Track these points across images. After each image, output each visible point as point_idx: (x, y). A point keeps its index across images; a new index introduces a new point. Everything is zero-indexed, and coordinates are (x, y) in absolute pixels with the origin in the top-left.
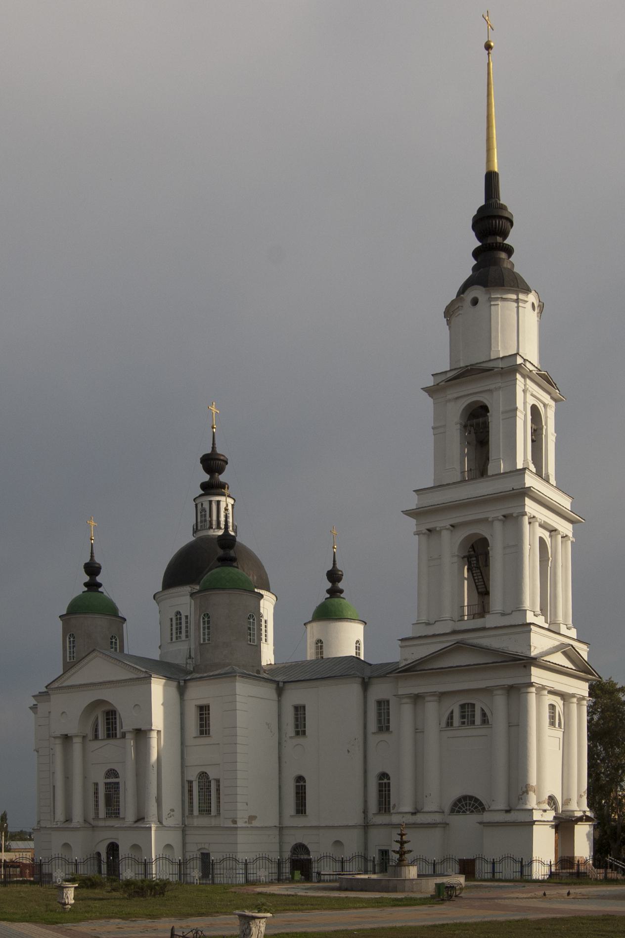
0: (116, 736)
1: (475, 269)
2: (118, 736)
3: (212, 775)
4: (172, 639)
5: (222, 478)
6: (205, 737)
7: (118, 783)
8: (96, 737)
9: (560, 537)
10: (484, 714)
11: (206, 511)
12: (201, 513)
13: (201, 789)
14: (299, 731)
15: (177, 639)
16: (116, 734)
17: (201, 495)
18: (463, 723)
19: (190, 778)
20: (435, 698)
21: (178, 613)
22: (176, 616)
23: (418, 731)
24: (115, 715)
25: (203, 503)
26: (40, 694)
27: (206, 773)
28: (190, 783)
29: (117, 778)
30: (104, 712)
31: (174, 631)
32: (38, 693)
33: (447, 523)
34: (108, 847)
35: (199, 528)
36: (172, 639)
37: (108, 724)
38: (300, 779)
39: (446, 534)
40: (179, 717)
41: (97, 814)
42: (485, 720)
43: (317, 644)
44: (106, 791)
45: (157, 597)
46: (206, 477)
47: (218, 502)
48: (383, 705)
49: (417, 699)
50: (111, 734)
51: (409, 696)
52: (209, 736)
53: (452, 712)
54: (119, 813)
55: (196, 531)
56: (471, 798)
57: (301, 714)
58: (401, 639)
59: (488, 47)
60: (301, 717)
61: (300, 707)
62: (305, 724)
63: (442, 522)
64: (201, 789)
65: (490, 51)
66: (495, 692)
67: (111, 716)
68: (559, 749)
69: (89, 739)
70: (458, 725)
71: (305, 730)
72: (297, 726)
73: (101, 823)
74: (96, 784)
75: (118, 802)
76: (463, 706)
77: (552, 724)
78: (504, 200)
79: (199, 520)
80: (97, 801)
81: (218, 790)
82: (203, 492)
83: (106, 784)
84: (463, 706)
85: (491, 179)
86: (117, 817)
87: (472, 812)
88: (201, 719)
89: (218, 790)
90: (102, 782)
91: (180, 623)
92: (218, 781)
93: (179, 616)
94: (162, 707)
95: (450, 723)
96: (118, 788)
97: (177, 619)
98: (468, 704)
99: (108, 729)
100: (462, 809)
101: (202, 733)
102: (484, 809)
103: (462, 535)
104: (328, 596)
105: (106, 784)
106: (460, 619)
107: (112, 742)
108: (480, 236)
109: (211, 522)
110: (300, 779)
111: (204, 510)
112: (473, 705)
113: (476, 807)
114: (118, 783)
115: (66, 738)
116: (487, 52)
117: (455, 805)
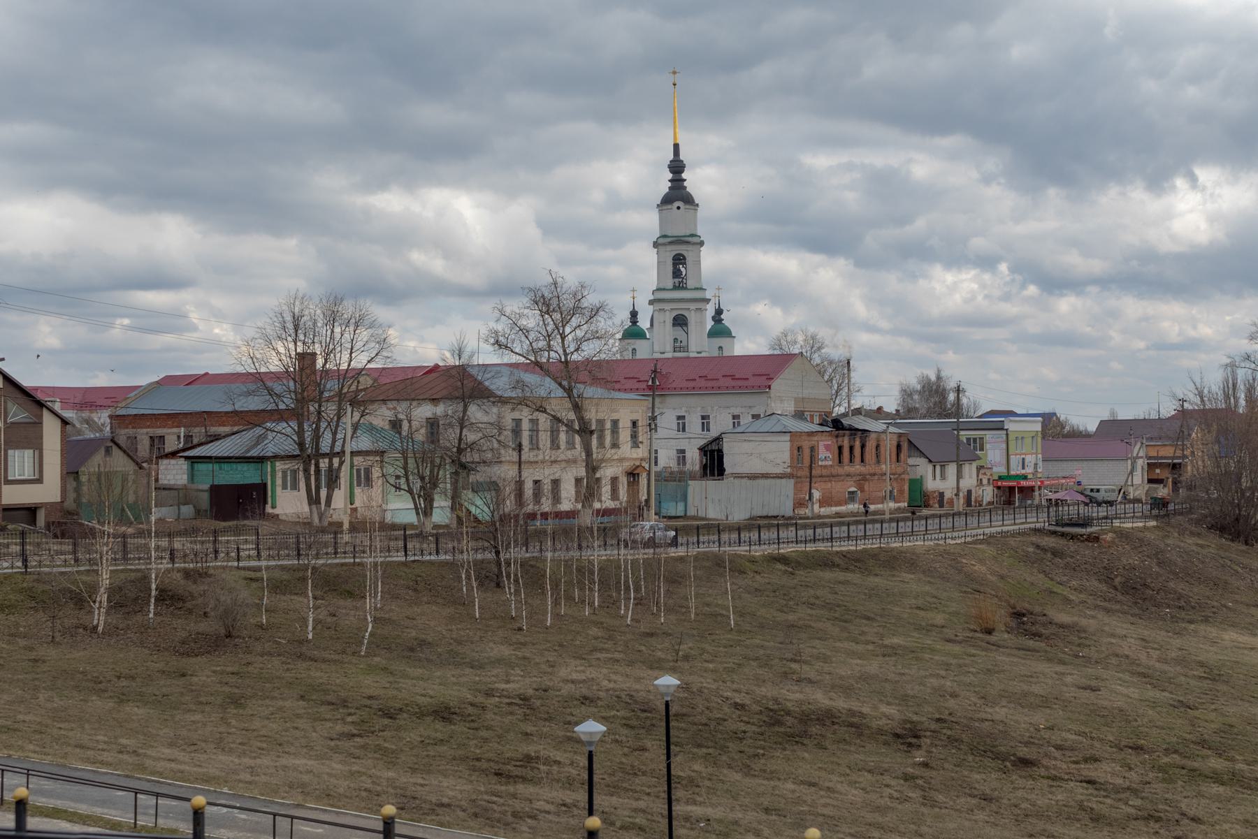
78: (682, 158)
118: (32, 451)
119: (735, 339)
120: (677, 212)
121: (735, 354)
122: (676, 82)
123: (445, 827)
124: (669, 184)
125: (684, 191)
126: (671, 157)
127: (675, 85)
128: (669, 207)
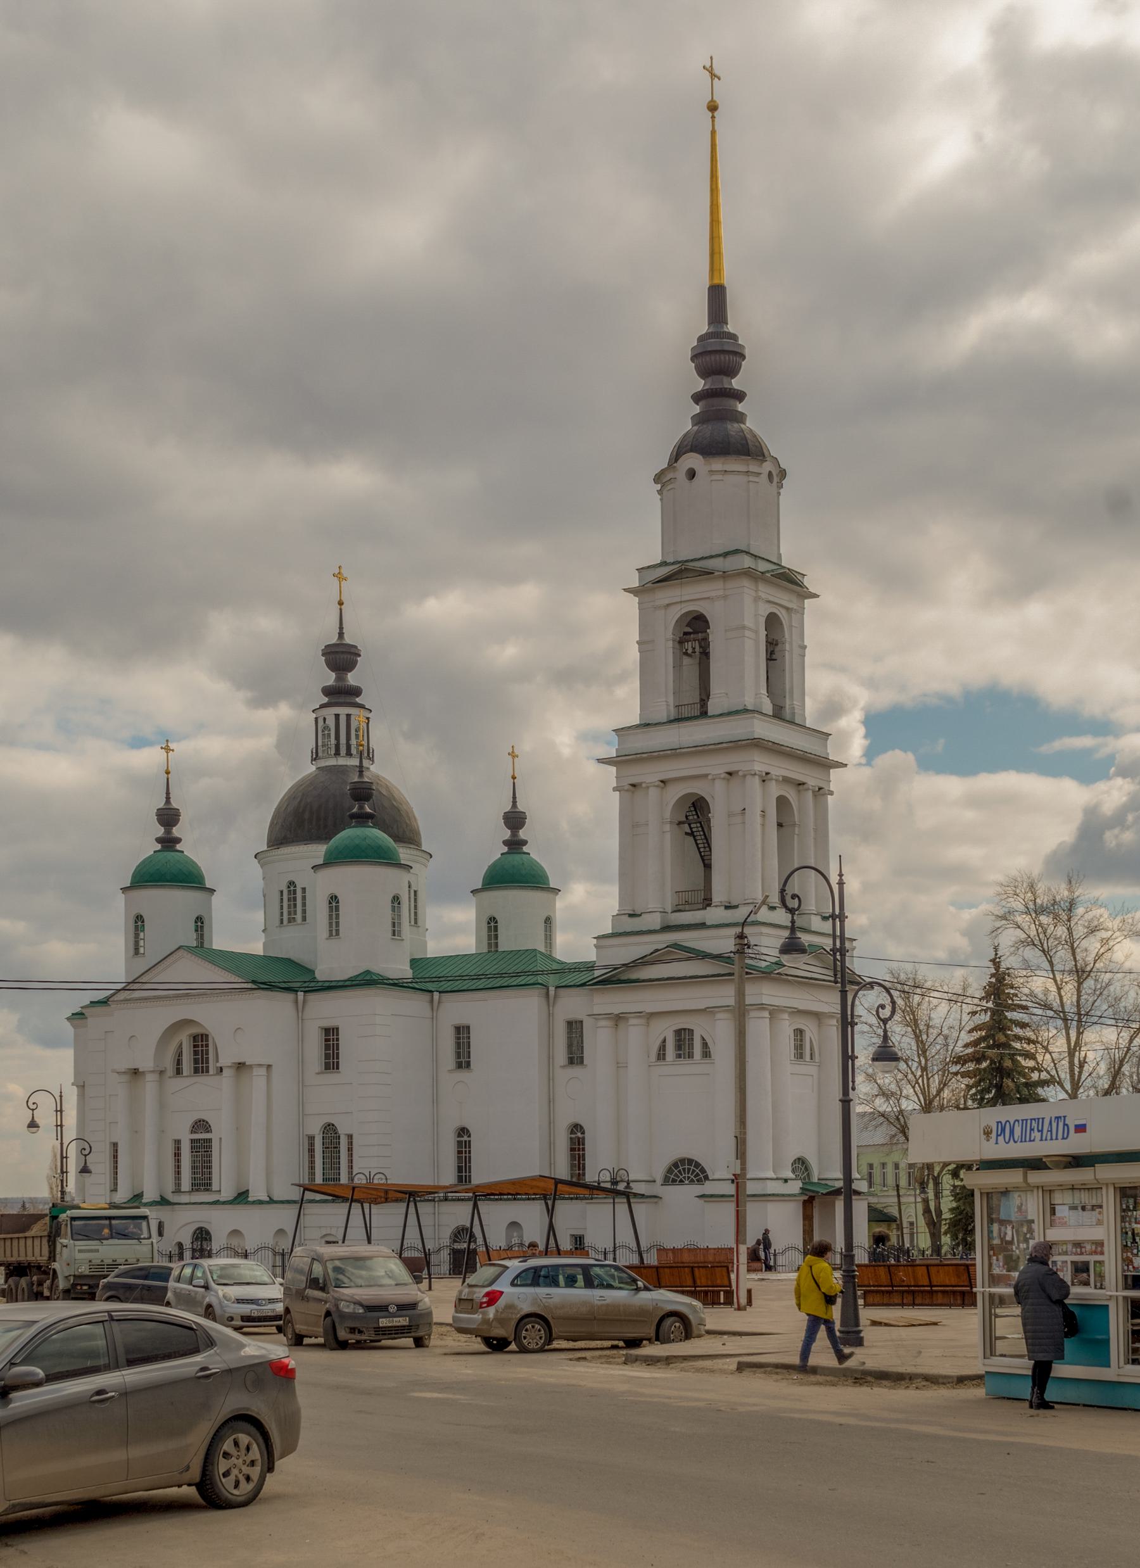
0: (207, 1071)
1: (698, 420)
2: (211, 1071)
3: (342, 1130)
4: (282, 921)
5: (352, 679)
6: (332, 1072)
7: (210, 1140)
8: (179, 1072)
9: (810, 793)
10: (705, 1045)
11: (330, 730)
12: (323, 731)
13: (337, 1148)
14: (462, 1062)
15: (289, 921)
16: (207, 1068)
17: (322, 706)
18: (679, 1056)
19: (310, 1133)
20: (642, 1021)
21: (292, 883)
22: (289, 887)
23: (620, 1065)
24: (207, 1040)
25: (326, 717)
26: (92, 1005)
27: (333, 1125)
28: (311, 1139)
29: (208, 1132)
30: (190, 1036)
33: (654, 778)
34: (195, 1233)
35: (320, 754)
36: (282, 921)
37: (196, 1053)
38: (463, 1131)
39: (653, 793)
41: (178, 1184)
42: (706, 1052)
43: (489, 923)
44: (192, 1152)
45: (259, 857)
46: (330, 678)
48: (574, 1028)
49: (618, 1019)
50: (201, 1066)
51: (608, 1016)
52: (338, 1072)
53: (664, 1041)
54: (210, 1184)
55: (315, 758)
56: (690, 1161)
57: (463, 1038)
58: (596, 936)
59: (713, 108)
60: (463, 1042)
61: (463, 1027)
62: (469, 1052)
63: (650, 774)
64: (337, 1148)
65: (716, 114)
66: (719, 1016)
67: (201, 1042)
68: (813, 1091)
69: (169, 1075)
70: (672, 1060)
71: (470, 1061)
72: (458, 1055)
73: (185, 1198)
74: (178, 1143)
75: (193, 1168)
76: (678, 1032)
77: (800, 1055)
79: (320, 743)
80: (179, 1167)
81: (350, 1150)
83: (192, 1141)
84: (678, 1032)
86: (208, 1190)
87: (692, 1181)
88: (327, 1047)
89: (350, 1150)
90: (186, 1138)
91: (295, 899)
92: (350, 1137)
93: (292, 888)
95: (661, 1055)
96: (210, 1147)
97: (289, 892)
98: (685, 1029)
99: (196, 1061)
100: (679, 1177)
101: (327, 1067)
102: (706, 1178)
103: (675, 793)
104: (506, 849)
105: (192, 1141)
106: (675, 909)
107: (201, 1079)
108: (704, 372)
109: (337, 746)
110: (463, 1131)
111: (326, 728)
112: (691, 1031)
113: (697, 1175)
114: (210, 1140)
115: (136, 1073)
116: (711, 114)
117: (670, 1171)
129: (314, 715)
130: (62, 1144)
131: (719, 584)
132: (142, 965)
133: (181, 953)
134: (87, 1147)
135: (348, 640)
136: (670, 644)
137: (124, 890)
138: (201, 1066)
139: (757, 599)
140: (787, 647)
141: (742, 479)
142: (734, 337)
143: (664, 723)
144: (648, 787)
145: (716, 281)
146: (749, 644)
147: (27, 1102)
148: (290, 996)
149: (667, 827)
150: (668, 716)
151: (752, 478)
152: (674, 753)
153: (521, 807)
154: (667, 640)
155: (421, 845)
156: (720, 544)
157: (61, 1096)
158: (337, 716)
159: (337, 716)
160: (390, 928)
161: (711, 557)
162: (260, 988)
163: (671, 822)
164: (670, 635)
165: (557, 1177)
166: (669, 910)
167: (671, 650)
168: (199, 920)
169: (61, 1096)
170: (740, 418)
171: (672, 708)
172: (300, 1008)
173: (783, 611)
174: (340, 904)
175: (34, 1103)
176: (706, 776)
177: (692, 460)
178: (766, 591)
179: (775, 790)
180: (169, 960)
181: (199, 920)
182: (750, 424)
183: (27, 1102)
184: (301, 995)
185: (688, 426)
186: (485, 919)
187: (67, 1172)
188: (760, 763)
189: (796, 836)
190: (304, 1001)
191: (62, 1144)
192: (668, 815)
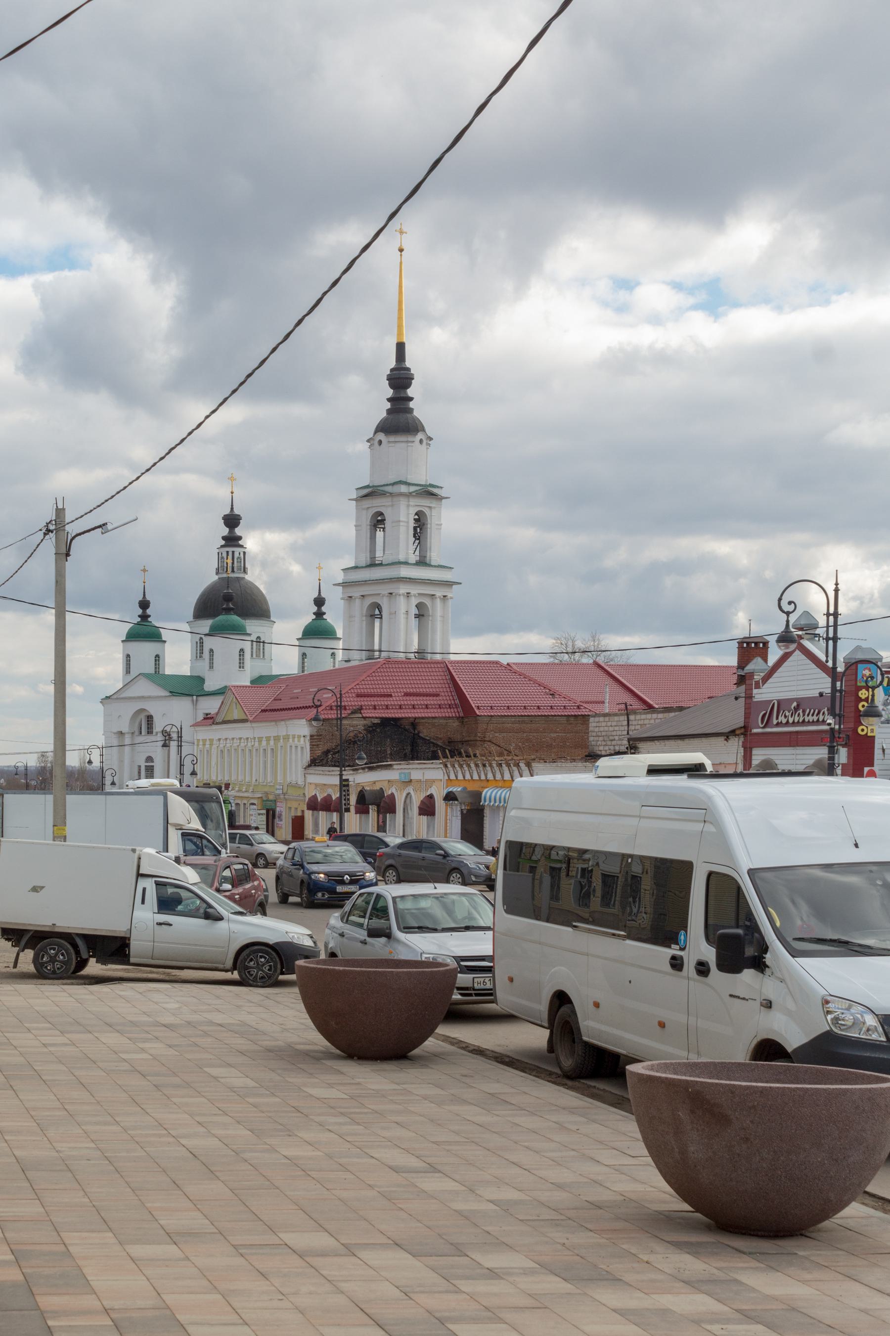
1: (389, 412)
2: (154, 734)
7: (153, 766)
8: (141, 733)
17: (222, 546)
31: (198, 652)
32: (741, 1054)
40: (667, 742)
47: (233, 552)
55: (217, 573)
63: (356, 592)
67: (150, 719)
74: (140, 767)
78: (408, 364)
82: (18, 948)
85: (401, 348)
90: (143, 765)
94: (769, 646)
103: (368, 601)
108: (392, 386)
111: (222, 558)
114: (153, 766)
118: (830, 692)
119: (166, 644)
120: (395, 446)
121: (276, 671)
122: (404, 247)
123: (679, 1063)
124: (388, 405)
125: (409, 415)
126: (392, 363)
127: (401, 250)
128: (410, 438)
129: (218, 551)
130: (181, 757)
131: (389, 499)
132: (130, 678)
133: (141, 677)
134: (195, 759)
135: (236, 512)
136: (369, 527)
137: (123, 641)
138: (150, 731)
139: (408, 506)
140: (429, 526)
141: (404, 445)
142: (408, 369)
143: (362, 567)
144: (355, 599)
145: (400, 341)
146: (402, 529)
147: (780, 600)
148: (190, 698)
149: (364, 618)
150: (366, 563)
151: (409, 444)
152: (365, 583)
153: (323, 595)
154: (367, 525)
155: (270, 616)
156: (392, 478)
157: (837, 591)
158: (228, 552)
159: (228, 552)
160: (238, 665)
161: (387, 485)
162: (174, 695)
163: (366, 616)
164: (368, 523)
165: (103, 797)
166: (364, 659)
167: (369, 530)
168: (157, 656)
169: (837, 591)
170: (410, 411)
171: (369, 559)
172: (195, 704)
173: (426, 509)
174: (214, 653)
175: (790, 603)
176: (379, 594)
177: (381, 436)
178: (413, 501)
179: (414, 601)
180: (135, 680)
181: (157, 656)
182: (415, 413)
183: (780, 600)
184: (195, 697)
185: (384, 414)
186: (301, 654)
187: (183, 774)
188: (403, 589)
189: (430, 622)
190: (197, 700)
191: (181, 757)
192: (364, 612)
